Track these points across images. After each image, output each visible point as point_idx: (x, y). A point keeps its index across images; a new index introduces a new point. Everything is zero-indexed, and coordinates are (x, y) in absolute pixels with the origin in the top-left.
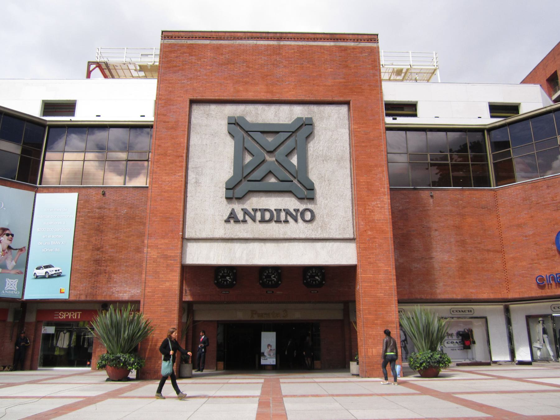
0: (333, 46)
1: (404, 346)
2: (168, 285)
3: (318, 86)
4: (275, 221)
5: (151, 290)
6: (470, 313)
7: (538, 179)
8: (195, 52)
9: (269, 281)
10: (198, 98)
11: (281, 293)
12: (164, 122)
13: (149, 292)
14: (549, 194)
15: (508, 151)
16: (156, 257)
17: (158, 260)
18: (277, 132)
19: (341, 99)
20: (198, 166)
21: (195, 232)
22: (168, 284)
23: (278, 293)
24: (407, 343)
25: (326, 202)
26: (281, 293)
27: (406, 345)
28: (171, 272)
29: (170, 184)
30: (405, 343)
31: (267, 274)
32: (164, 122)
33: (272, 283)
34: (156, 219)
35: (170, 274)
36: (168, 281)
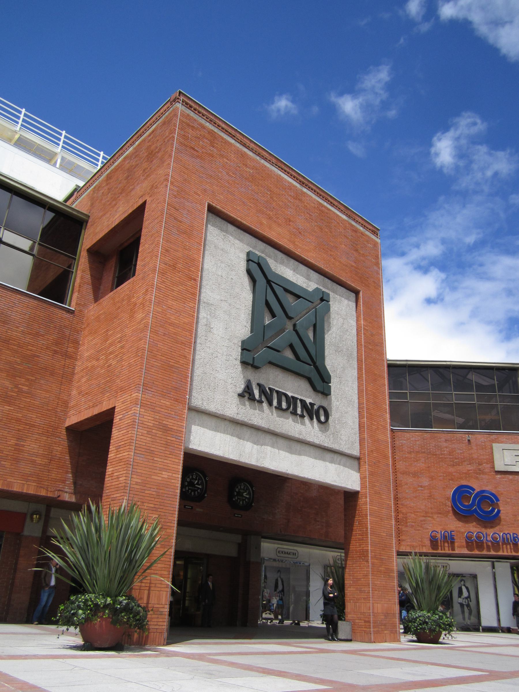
0: (346, 220)
1: (467, 603)
2: (166, 476)
3: (334, 259)
4: (291, 413)
5: (139, 481)
6: (294, 556)
7: (408, 430)
8: (217, 144)
9: (192, 491)
10: (217, 207)
11: (202, 510)
12: (175, 219)
13: (137, 483)
14: (446, 447)
15: (474, 398)
16: (152, 425)
17: (154, 431)
18: (298, 297)
19: (353, 285)
20: (211, 302)
21: (202, 399)
22: (165, 475)
23: (198, 510)
24: (471, 601)
25: (338, 403)
26: (202, 510)
27: (470, 603)
28: (171, 456)
29: (177, 314)
30: (468, 601)
31: (190, 481)
32: (175, 219)
33: (195, 493)
34: (156, 363)
35: (170, 459)
36: (166, 470)
